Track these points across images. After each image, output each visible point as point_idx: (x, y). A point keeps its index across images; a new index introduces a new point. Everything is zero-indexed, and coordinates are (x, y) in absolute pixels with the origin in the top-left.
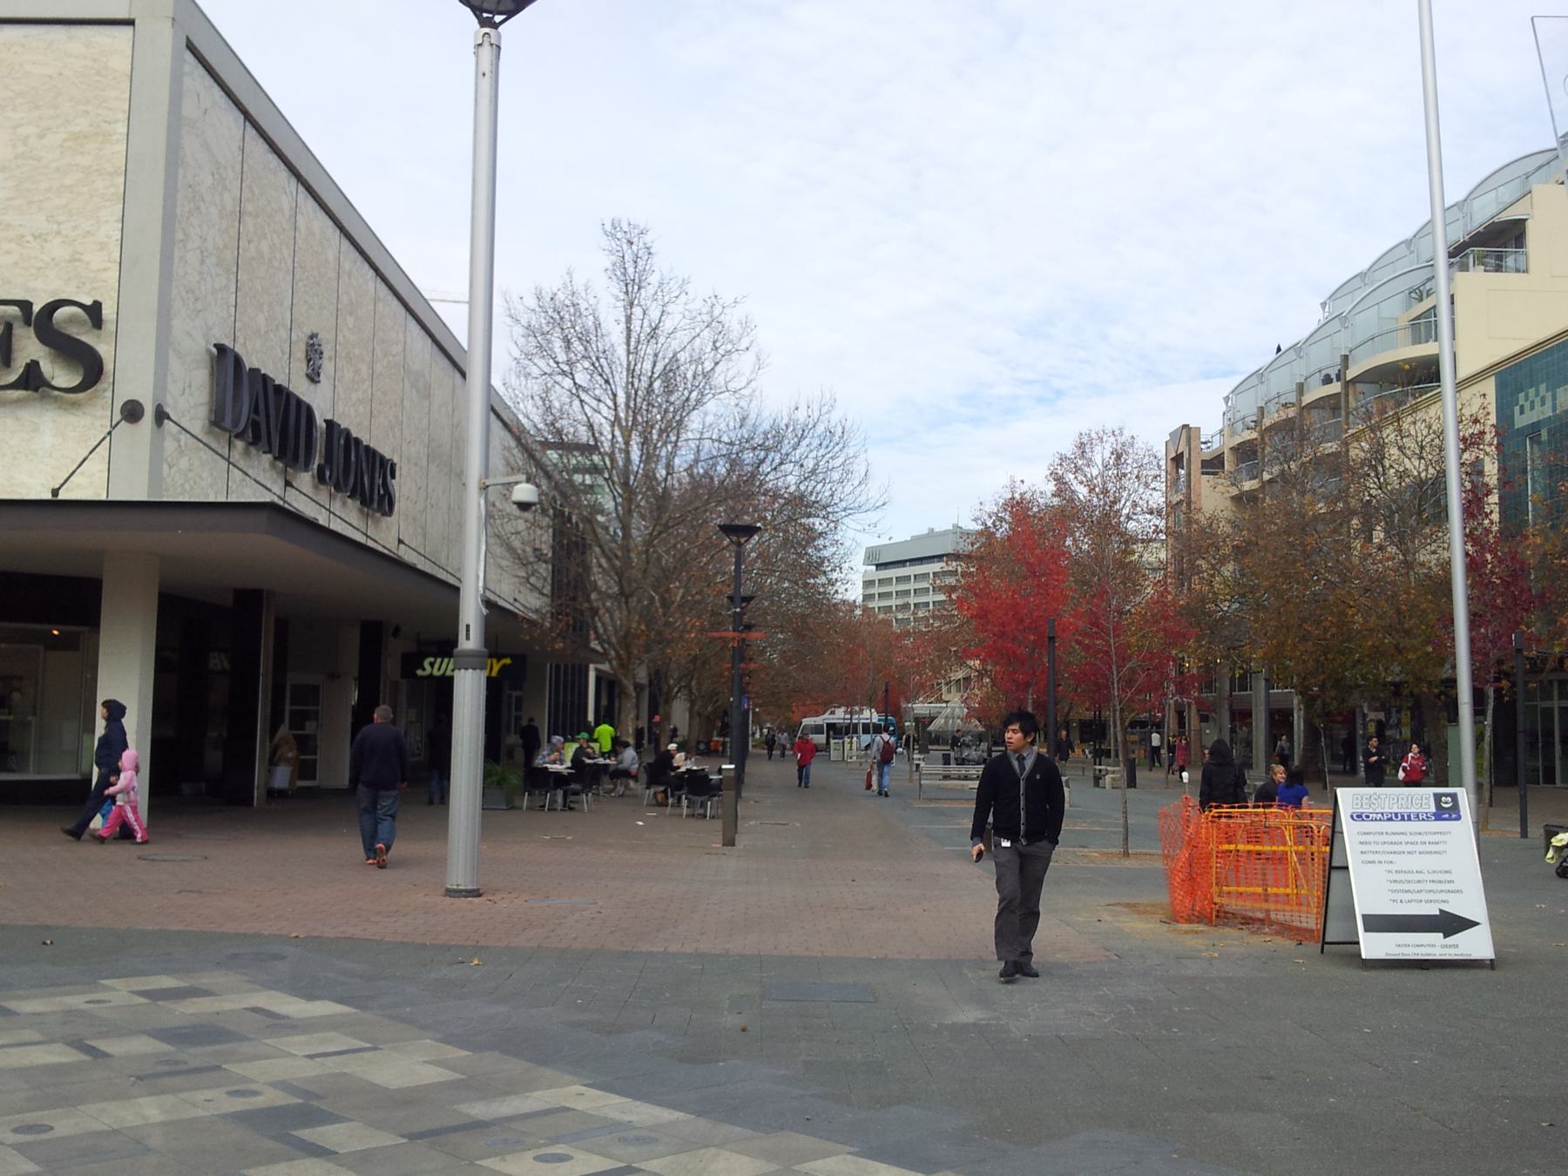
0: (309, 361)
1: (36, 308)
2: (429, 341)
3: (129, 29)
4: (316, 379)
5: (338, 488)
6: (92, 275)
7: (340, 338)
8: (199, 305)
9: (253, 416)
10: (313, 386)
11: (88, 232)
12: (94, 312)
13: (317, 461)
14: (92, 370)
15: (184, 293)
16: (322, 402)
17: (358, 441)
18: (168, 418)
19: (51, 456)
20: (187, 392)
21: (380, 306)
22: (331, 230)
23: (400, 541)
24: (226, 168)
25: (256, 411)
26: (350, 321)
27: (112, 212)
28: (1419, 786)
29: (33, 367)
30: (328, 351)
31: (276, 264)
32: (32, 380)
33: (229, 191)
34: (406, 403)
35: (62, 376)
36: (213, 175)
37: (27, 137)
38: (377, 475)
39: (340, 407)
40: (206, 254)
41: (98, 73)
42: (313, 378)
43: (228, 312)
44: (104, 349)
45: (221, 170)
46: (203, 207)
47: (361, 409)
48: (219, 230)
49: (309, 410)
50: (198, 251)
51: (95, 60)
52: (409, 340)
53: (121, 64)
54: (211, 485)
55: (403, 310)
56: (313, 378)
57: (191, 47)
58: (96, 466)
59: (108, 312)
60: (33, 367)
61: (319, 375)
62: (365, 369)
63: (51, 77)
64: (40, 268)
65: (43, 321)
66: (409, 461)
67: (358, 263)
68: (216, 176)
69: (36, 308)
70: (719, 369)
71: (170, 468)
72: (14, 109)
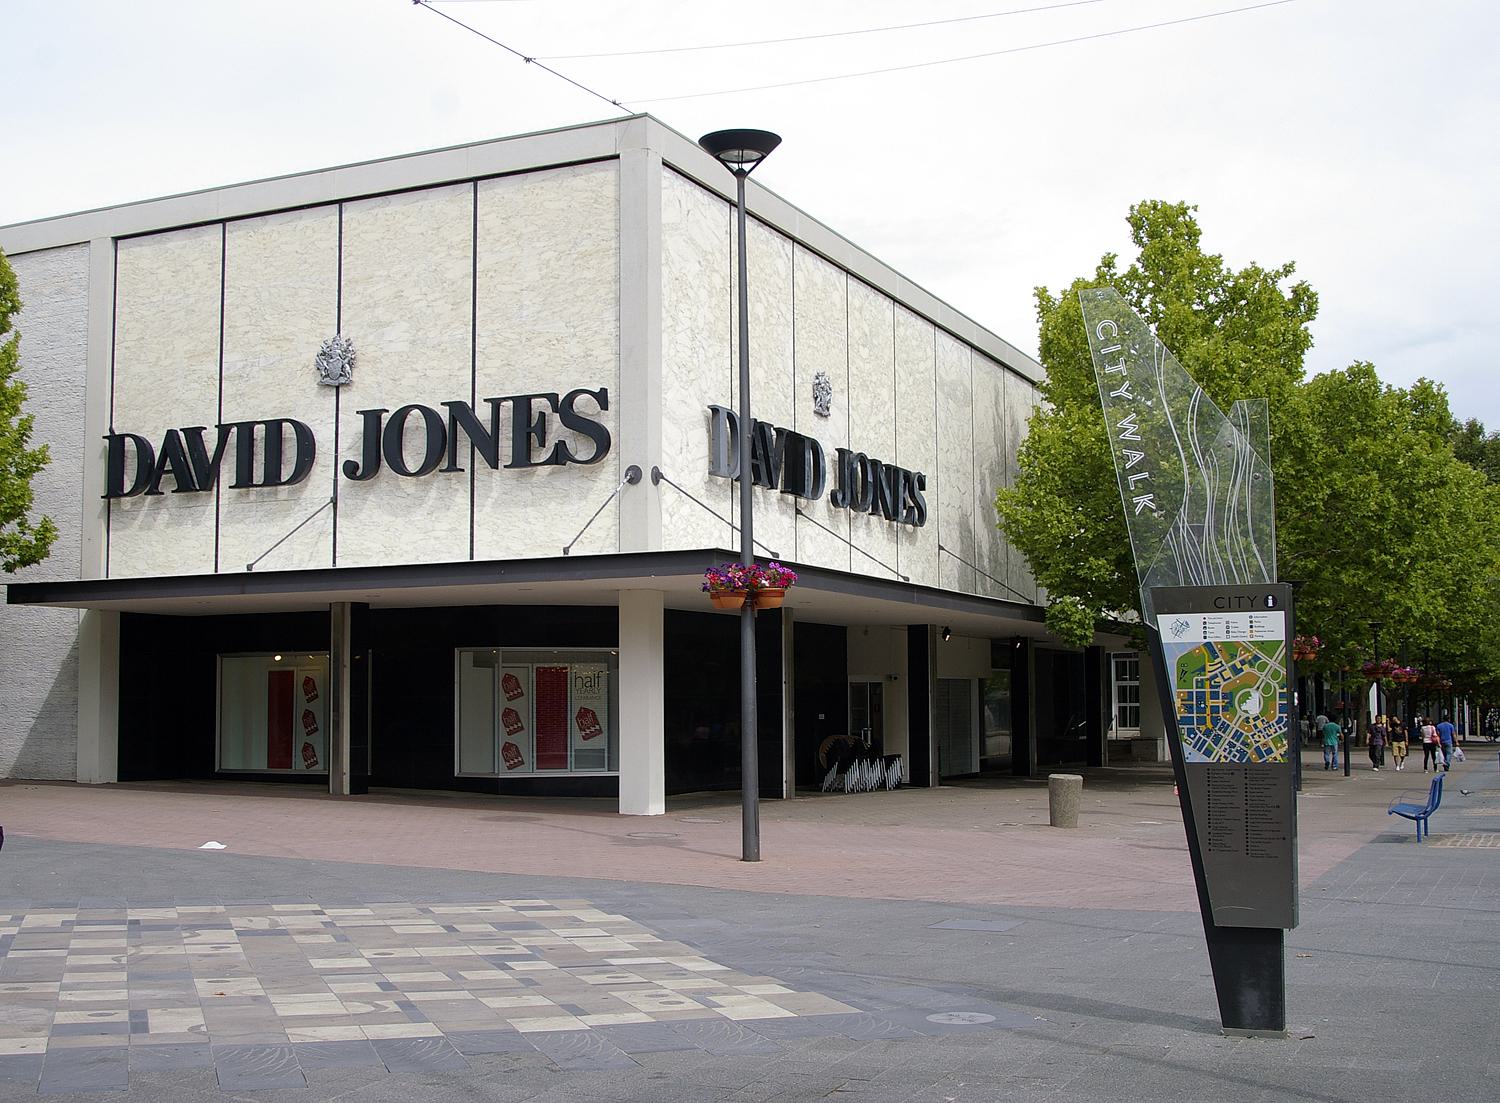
0: (816, 398)
1: (561, 398)
2: (967, 350)
3: (604, 174)
4: (825, 413)
5: (854, 506)
6: (600, 366)
7: (853, 369)
8: (692, 376)
9: (755, 461)
10: (822, 421)
11: (596, 332)
12: (602, 398)
13: (830, 483)
14: (603, 443)
15: (675, 369)
16: (830, 437)
17: (875, 463)
18: (663, 478)
19: (578, 515)
20: (684, 450)
21: (901, 331)
22: (835, 274)
23: (941, 548)
24: (712, 254)
25: (754, 455)
26: (865, 352)
27: (610, 315)
28: (279, 672)
29: (561, 447)
30: (837, 386)
31: (773, 321)
32: (560, 456)
33: (717, 271)
34: (941, 415)
35: (582, 449)
36: (699, 262)
37: (549, 261)
38: (901, 489)
39: (857, 433)
40: (697, 331)
41: (596, 201)
42: (822, 412)
43: (723, 375)
44: (610, 426)
45: (709, 257)
46: (691, 294)
47: (883, 430)
48: (709, 307)
49: (815, 447)
50: (688, 331)
51: (593, 192)
52: (939, 353)
53: (610, 191)
54: (715, 525)
55: (930, 328)
56: (822, 412)
57: (665, 164)
58: (606, 520)
59: (611, 396)
60: (561, 447)
61: (828, 409)
62: (885, 394)
63: (563, 210)
64: (562, 366)
65: (564, 406)
66: (948, 469)
67: (871, 297)
68: (702, 263)
69: (561, 398)
70: (609, 525)
71: (671, 516)
72: (538, 241)
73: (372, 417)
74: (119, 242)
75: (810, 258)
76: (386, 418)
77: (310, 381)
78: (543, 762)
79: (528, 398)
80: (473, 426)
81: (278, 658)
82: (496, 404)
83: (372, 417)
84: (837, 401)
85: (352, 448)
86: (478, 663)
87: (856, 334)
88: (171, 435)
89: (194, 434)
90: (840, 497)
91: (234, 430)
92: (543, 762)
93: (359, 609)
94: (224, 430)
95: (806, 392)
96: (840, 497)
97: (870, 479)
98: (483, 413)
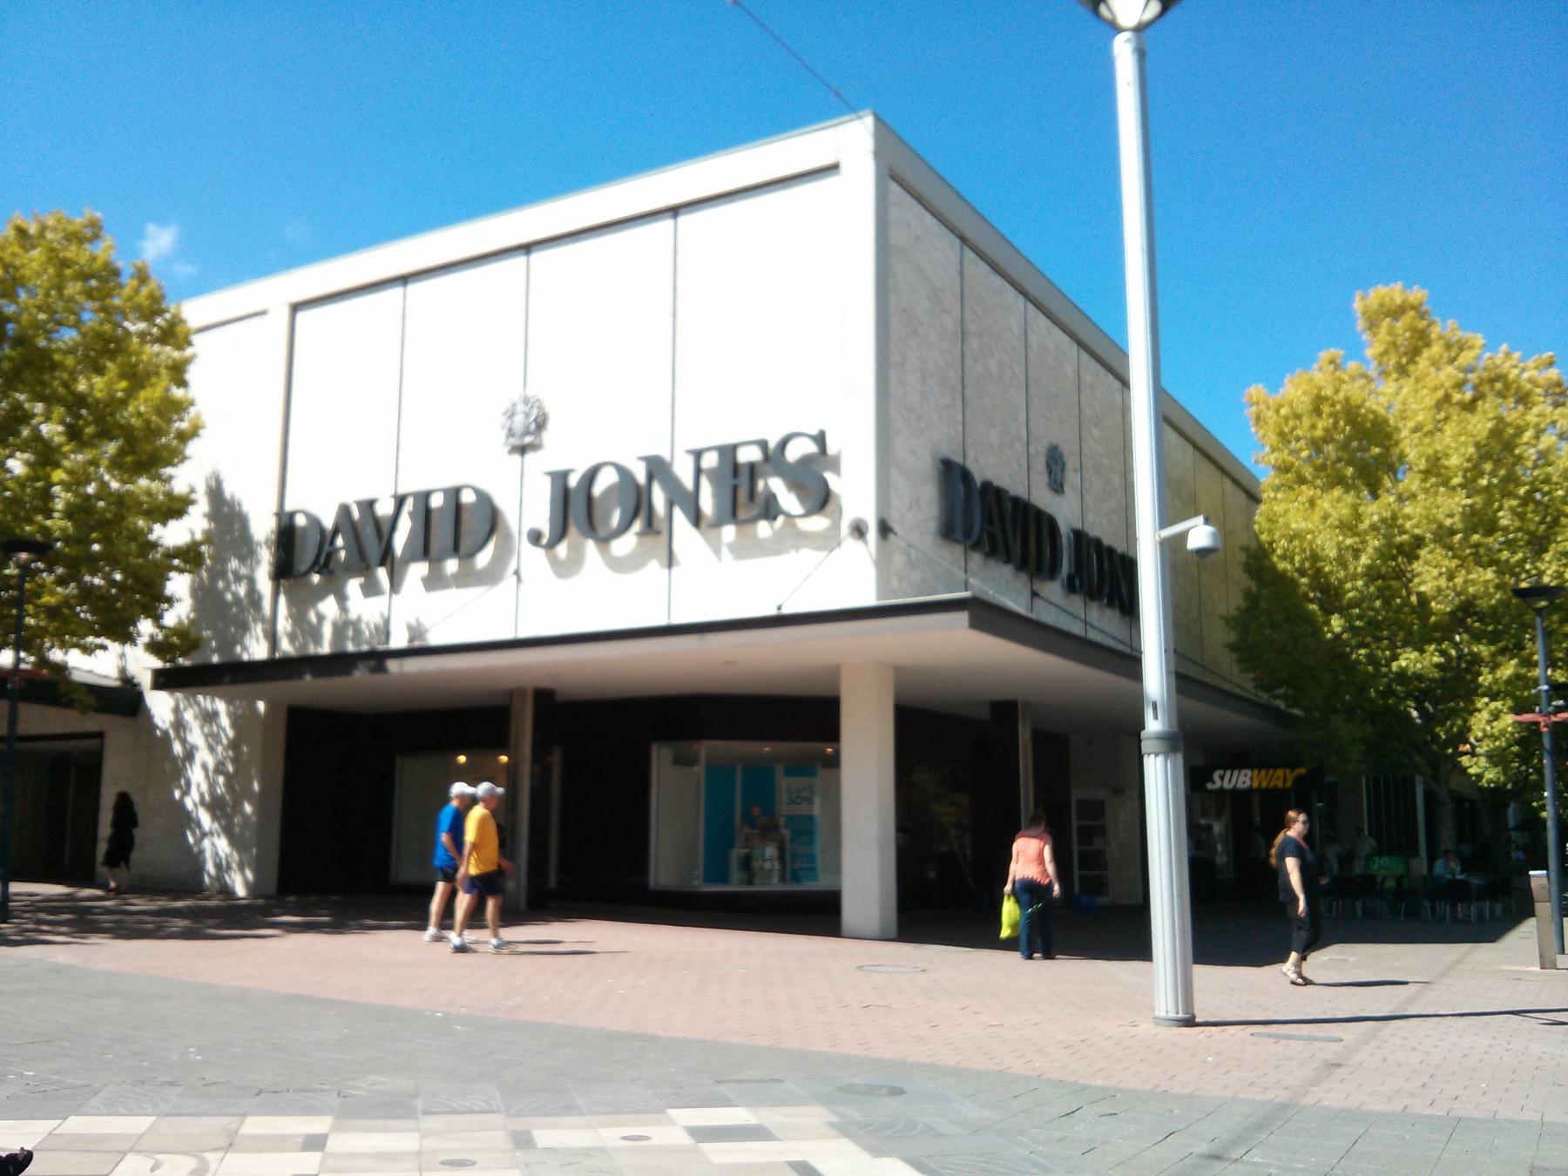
2: (1190, 449)
26: (1096, 432)
30: (1071, 463)
39: (1090, 518)
42: (1057, 487)
56: (1057, 487)
73: (560, 478)
74: (302, 316)
75: (1042, 319)
76: (573, 481)
77: (498, 442)
78: (708, 879)
79: (733, 448)
80: (672, 485)
81: (462, 759)
82: (698, 455)
83: (560, 478)
84: (1072, 479)
85: (540, 515)
86: (683, 761)
87: (1088, 411)
88: (345, 510)
89: (368, 506)
90: (1077, 583)
91: (1005, 932)
92: (708, 879)
93: (545, 699)
94: (400, 501)
95: (1040, 464)
96: (1077, 583)
97: (1106, 566)
98: (684, 471)
